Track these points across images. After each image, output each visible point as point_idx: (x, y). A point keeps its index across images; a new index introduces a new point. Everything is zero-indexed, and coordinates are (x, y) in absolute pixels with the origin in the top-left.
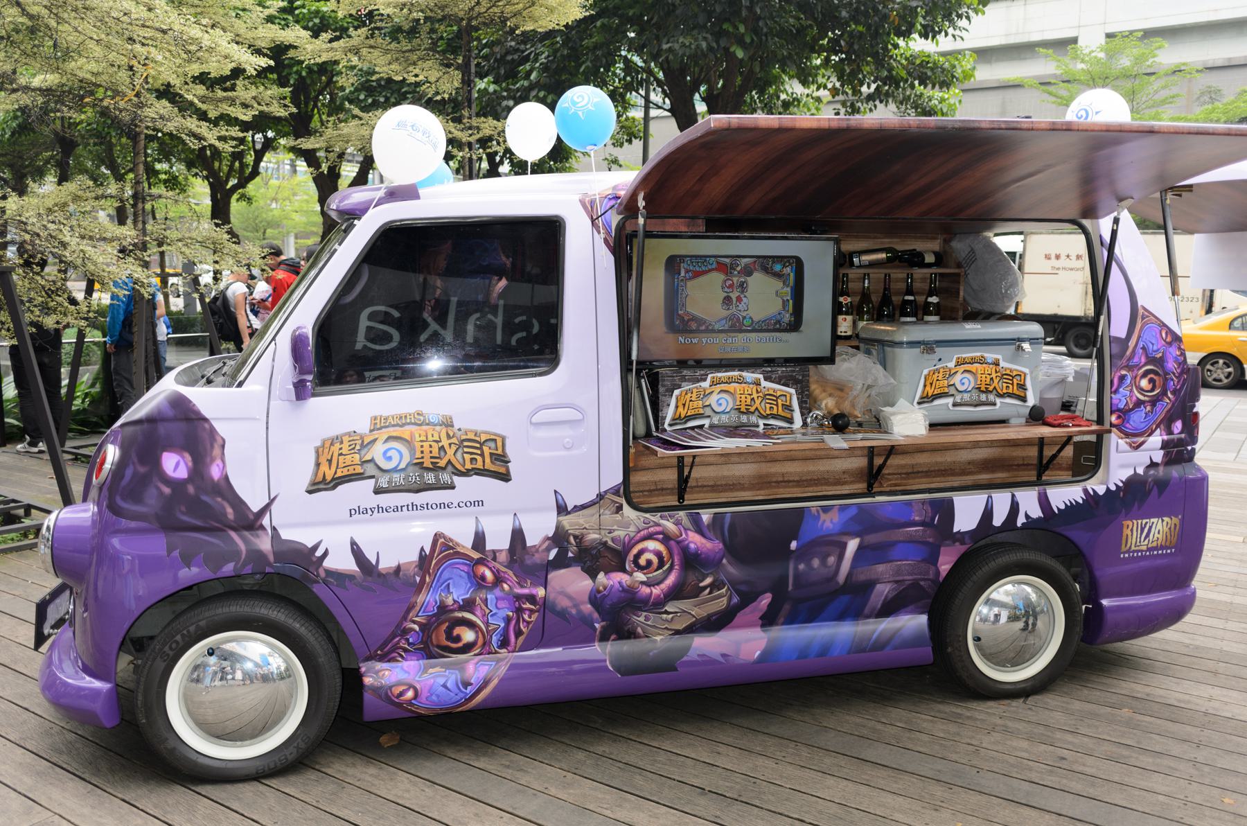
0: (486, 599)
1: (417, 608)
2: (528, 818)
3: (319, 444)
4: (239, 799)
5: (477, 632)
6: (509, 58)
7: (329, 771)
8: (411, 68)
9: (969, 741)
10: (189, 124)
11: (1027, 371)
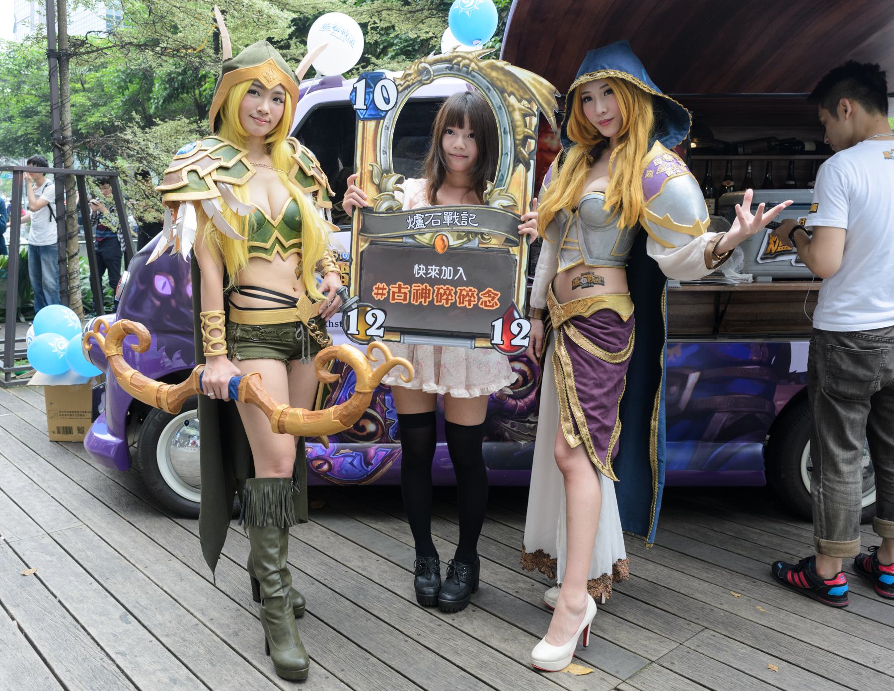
0: (385, 399)
5: (377, 425)
9: (788, 551)
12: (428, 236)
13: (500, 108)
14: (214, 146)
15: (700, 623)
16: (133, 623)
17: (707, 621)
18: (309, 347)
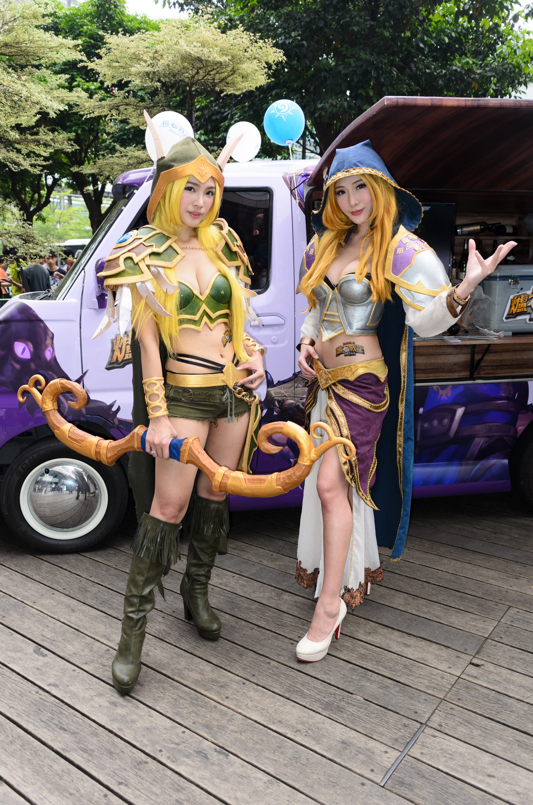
2: (251, 577)
3: (113, 337)
4: (67, 563)
6: (214, 118)
7: (122, 549)
10: (11, 155)
14: (149, 233)
15: (504, 603)
16: (49, 656)
17: (508, 601)
18: (233, 408)
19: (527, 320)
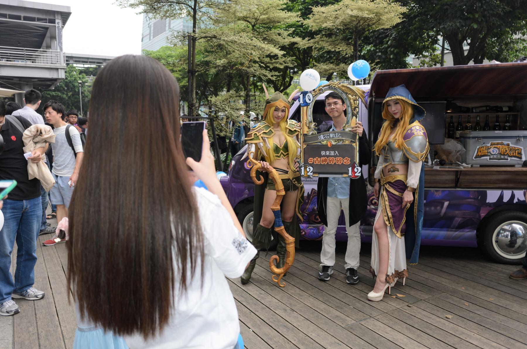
1: (307, 209)
6: (381, 36)
8: (337, 46)
11: (522, 148)
12: (325, 142)
13: (346, 99)
19: (488, 159)
